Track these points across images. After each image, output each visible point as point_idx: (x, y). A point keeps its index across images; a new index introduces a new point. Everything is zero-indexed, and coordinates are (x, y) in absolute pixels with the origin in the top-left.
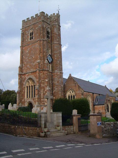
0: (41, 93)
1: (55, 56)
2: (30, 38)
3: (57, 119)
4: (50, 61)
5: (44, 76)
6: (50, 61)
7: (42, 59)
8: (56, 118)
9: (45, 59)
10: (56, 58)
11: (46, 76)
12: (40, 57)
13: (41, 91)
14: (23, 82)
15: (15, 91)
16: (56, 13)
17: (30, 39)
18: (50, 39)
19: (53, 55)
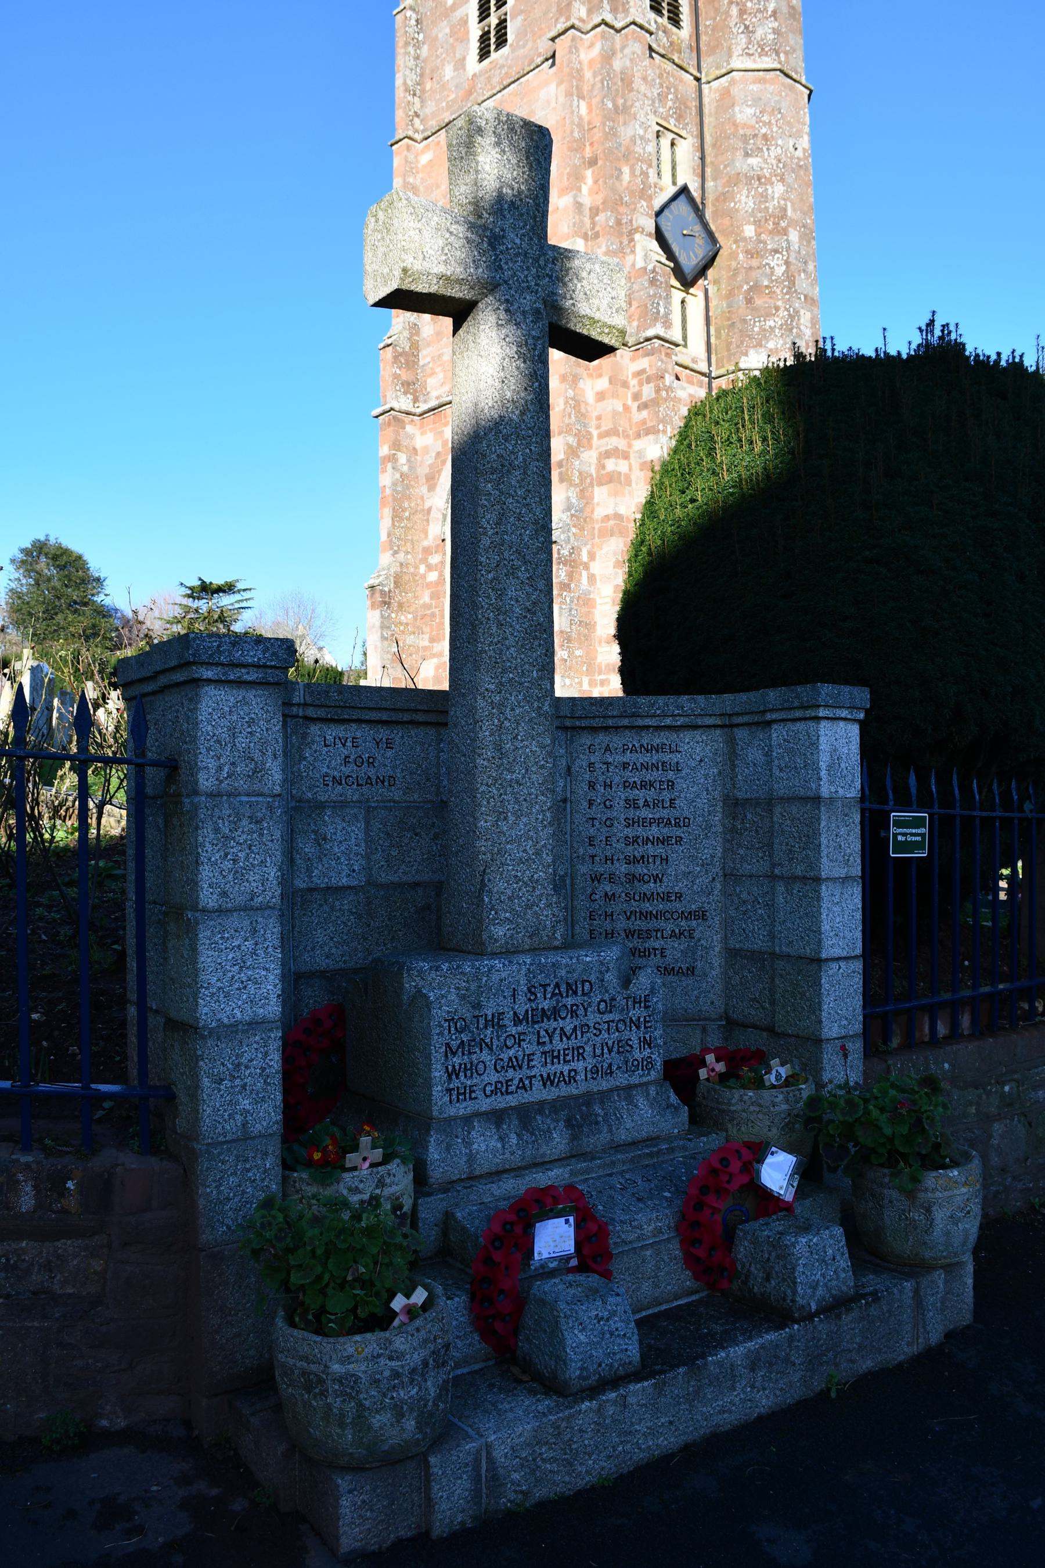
0: (592, 578)
1: (745, 201)
2: (484, 38)
3: (729, 876)
4: (689, 261)
5: (626, 408)
6: (689, 261)
7: (597, 235)
8: (713, 848)
9: (636, 230)
10: (749, 231)
11: (644, 406)
12: (579, 206)
13: (595, 568)
14: (424, 490)
15: (963, 345)
16: (473, 421)
17: (484, 53)
18: (685, 32)
19: (725, 197)
